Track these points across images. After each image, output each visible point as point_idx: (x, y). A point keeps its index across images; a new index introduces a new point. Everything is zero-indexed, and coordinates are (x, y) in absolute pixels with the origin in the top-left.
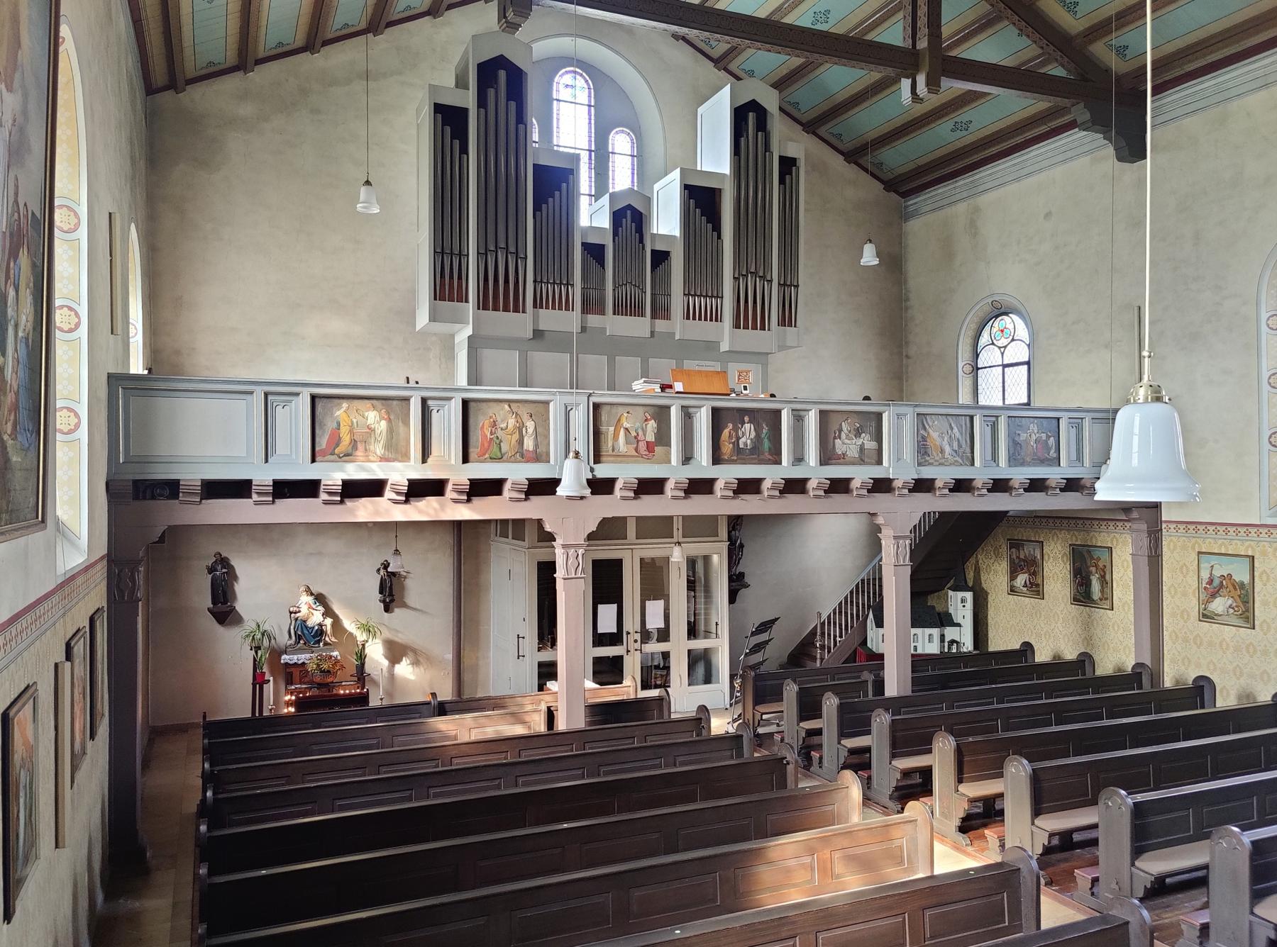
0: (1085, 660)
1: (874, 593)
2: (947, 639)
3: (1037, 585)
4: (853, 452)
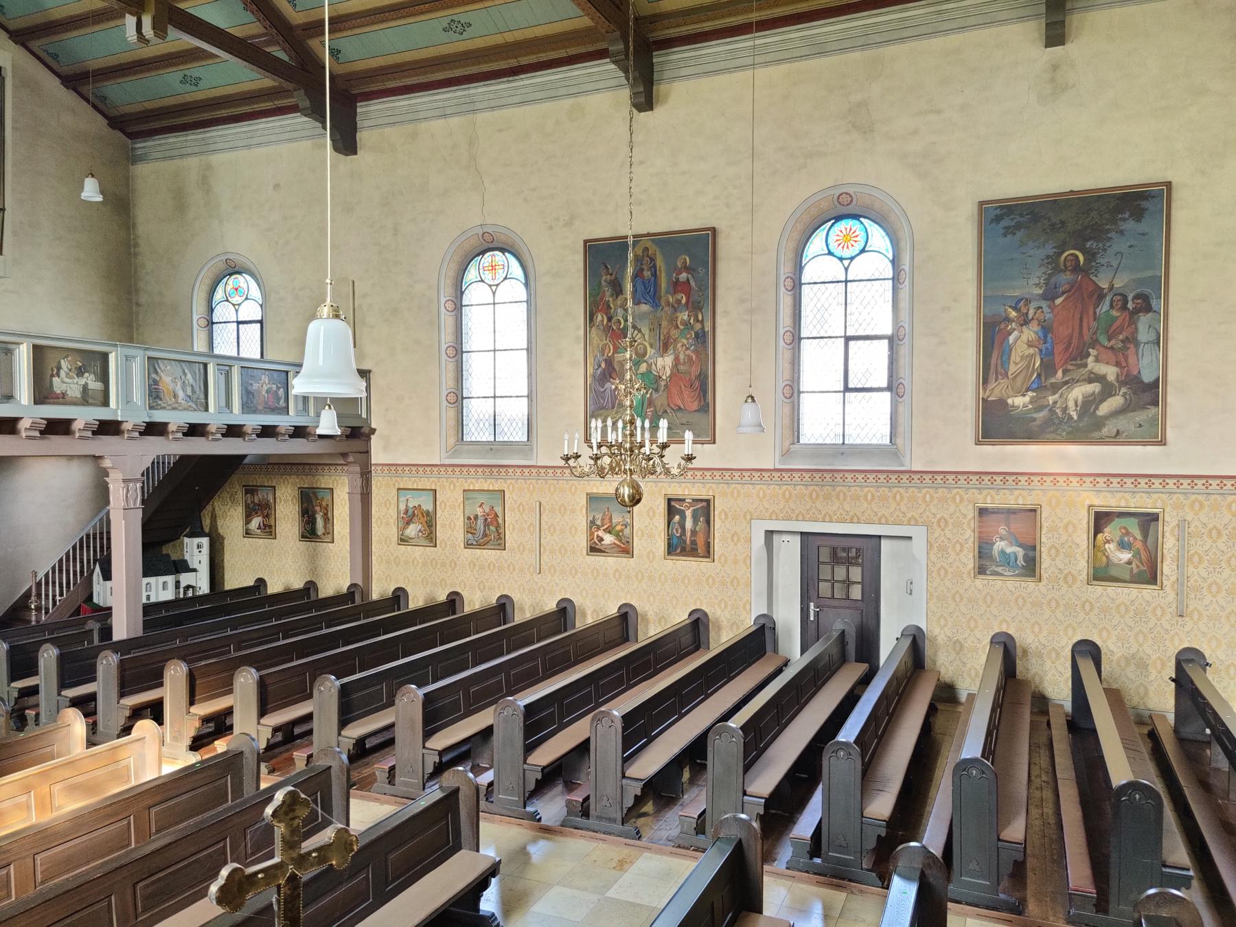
0: (311, 587)
1: (102, 547)
2: (183, 585)
3: (270, 527)
4: (74, 391)
